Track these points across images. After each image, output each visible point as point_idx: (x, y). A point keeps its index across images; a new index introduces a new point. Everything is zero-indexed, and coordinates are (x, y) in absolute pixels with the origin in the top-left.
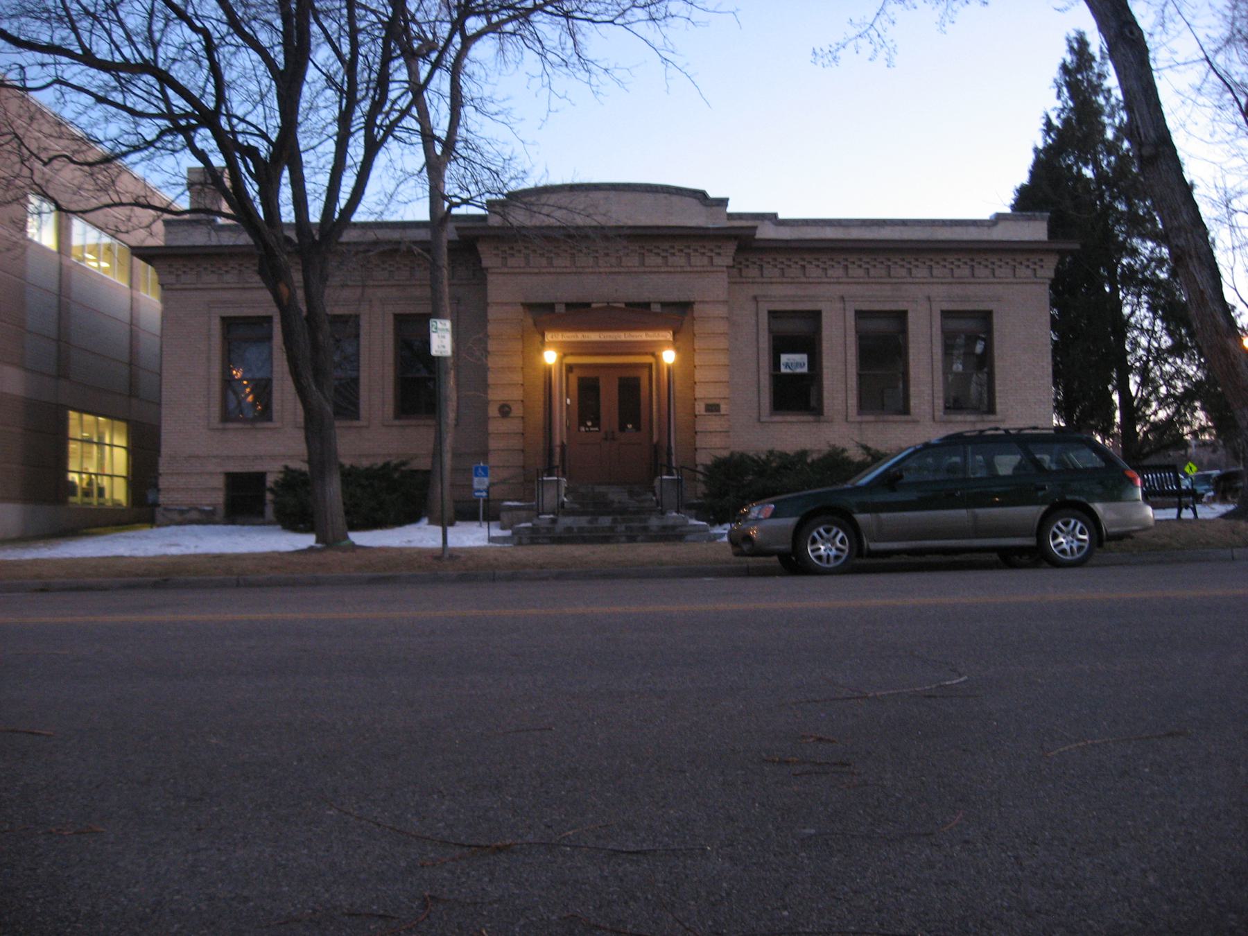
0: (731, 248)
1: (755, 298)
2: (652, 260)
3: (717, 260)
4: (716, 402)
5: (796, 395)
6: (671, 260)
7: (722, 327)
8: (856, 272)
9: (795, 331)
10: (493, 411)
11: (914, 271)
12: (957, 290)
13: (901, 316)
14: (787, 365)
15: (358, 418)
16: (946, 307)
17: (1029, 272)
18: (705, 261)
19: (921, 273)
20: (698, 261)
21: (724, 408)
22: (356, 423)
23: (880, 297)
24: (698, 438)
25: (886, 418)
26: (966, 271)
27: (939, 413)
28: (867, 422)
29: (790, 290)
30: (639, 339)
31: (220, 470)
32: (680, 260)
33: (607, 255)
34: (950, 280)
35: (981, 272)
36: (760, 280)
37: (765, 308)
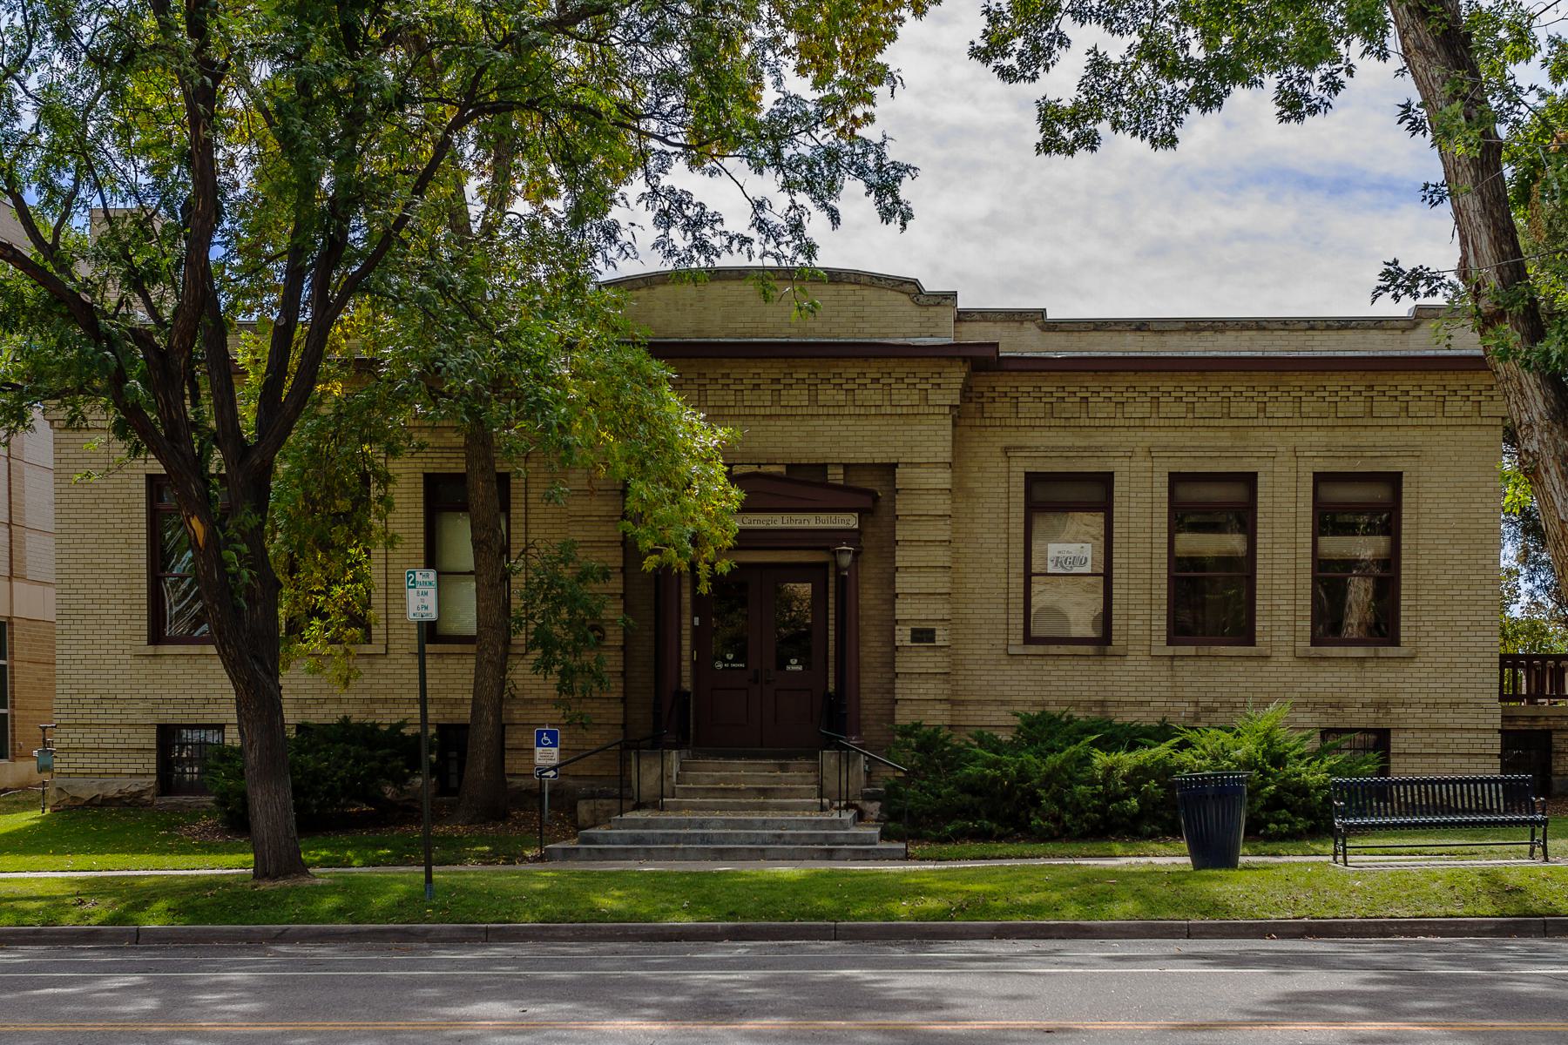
0: (956, 376)
1: (1006, 450)
2: (828, 395)
3: (935, 397)
4: (930, 626)
5: (1209, 606)
6: (861, 395)
7: (942, 505)
8: (1170, 408)
9: (1214, 502)
10: (903, 636)
11: (1270, 408)
12: (1343, 437)
13: (1250, 479)
14: (1057, 562)
15: (1396, 642)
16: (1324, 466)
17: (1468, 407)
18: (915, 397)
19: (1281, 409)
20: (905, 397)
21: (941, 637)
22: (1391, 651)
23: (1209, 448)
24: (898, 683)
25: (1215, 650)
26: (1358, 406)
27: (1304, 644)
28: (1182, 657)
29: (1067, 439)
30: (805, 525)
31: (152, 719)
32: (872, 396)
33: (757, 387)
34: (1330, 422)
35: (1385, 407)
36: (1013, 422)
37: (1020, 467)
